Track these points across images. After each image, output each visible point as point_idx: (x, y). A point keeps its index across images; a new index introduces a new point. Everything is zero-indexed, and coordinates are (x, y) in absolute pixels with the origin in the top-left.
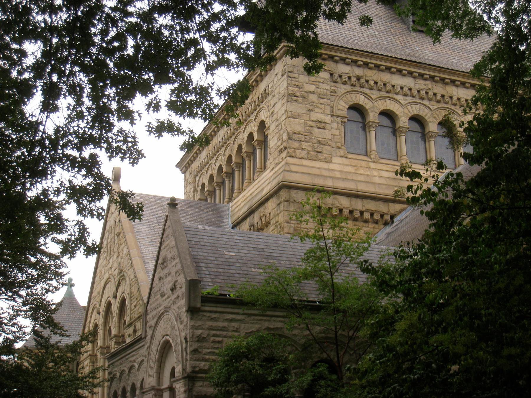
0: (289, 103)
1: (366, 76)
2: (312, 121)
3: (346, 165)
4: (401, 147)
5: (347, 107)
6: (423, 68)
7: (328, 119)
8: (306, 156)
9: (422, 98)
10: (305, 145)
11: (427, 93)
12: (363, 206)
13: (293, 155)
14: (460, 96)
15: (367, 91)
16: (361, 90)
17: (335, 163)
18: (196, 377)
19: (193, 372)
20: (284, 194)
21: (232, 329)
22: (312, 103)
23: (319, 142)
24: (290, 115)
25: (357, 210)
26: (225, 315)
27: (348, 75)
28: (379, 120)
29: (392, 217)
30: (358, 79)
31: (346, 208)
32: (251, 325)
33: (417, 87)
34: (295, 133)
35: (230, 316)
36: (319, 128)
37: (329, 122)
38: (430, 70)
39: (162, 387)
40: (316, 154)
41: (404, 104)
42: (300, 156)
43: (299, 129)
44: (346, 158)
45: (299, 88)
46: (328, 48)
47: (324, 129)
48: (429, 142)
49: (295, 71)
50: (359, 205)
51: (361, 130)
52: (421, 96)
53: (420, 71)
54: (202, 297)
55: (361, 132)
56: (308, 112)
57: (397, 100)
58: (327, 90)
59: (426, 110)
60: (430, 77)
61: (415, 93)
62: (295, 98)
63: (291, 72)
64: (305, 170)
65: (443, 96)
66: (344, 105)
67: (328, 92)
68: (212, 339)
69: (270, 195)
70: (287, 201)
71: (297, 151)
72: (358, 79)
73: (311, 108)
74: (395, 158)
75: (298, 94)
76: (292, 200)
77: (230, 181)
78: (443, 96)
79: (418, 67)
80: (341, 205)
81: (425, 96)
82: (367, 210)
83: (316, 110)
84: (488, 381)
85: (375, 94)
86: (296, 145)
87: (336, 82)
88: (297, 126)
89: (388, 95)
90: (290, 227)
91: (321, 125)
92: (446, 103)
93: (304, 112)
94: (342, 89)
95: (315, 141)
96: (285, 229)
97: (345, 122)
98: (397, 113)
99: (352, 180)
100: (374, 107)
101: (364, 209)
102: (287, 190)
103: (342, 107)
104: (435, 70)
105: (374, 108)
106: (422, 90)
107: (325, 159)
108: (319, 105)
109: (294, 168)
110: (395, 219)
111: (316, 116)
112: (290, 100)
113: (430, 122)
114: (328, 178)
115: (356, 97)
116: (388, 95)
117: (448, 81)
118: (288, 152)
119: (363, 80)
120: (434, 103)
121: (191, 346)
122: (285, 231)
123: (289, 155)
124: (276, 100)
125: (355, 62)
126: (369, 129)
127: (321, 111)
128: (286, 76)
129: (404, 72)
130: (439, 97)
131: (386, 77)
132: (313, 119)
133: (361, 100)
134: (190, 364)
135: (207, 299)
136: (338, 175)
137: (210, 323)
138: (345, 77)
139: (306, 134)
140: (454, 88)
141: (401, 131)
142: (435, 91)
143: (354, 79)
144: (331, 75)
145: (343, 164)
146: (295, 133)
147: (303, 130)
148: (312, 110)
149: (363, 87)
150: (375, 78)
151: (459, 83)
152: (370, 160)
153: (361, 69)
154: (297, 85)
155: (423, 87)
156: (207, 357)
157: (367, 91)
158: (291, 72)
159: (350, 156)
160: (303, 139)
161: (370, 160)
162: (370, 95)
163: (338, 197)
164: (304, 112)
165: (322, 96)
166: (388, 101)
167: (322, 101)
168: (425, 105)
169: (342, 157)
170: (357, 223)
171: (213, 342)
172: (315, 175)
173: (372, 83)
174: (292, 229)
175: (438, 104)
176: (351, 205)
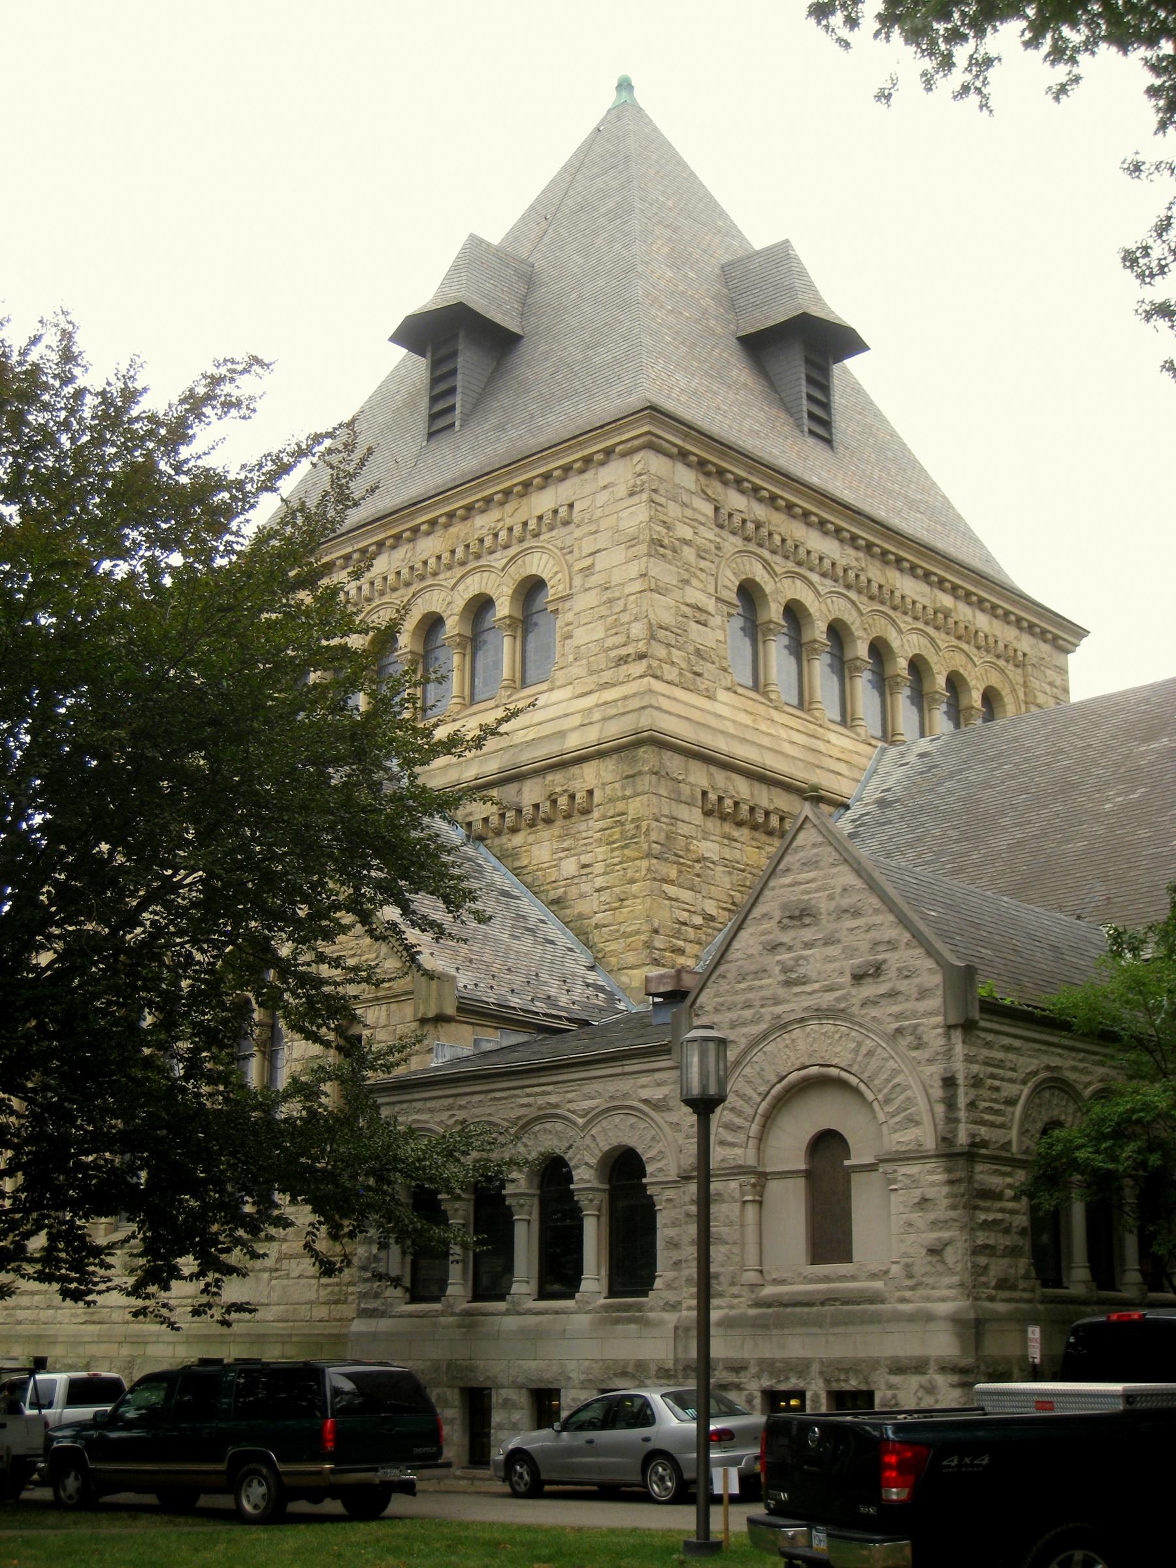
0: (652, 559)
1: (770, 523)
2: (688, 605)
3: (739, 709)
4: (810, 682)
7: (710, 605)
8: (677, 680)
10: (676, 655)
11: (857, 576)
12: (771, 800)
13: (659, 674)
14: (907, 592)
15: (766, 554)
16: (759, 551)
17: (721, 703)
18: (977, 1155)
19: (973, 1145)
20: (648, 757)
21: (1009, 1065)
22: (687, 567)
23: (698, 652)
24: (653, 587)
25: (760, 807)
26: (1001, 1037)
27: (743, 516)
30: (758, 526)
31: (745, 801)
32: (1029, 1060)
33: (844, 562)
34: (661, 627)
35: (1007, 1041)
36: (698, 622)
37: (713, 612)
39: (768, 1170)
40: (691, 680)
42: (669, 678)
43: (668, 618)
44: (735, 692)
45: (668, 528)
46: (722, 453)
47: (705, 625)
48: (851, 678)
49: (662, 491)
50: (764, 797)
54: (980, 1001)
56: (680, 585)
57: (812, 584)
58: (710, 541)
59: (854, 613)
62: (662, 550)
63: (655, 491)
64: (682, 710)
66: (732, 578)
67: (712, 546)
68: (989, 1082)
69: (598, 751)
70: (656, 773)
71: (664, 665)
72: (758, 526)
73: (686, 576)
75: (666, 541)
76: (663, 773)
79: (852, 521)
80: (738, 793)
82: (777, 810)
83: (694, 582)
86: (661, 652)
87: (721, 527)
88: (663, 610)
89: (797, 569)
90: (661, 829)
91: (700, 616)
92: (883, 603)
93: (675, 582)
94: (733, 543)
95: (691, 649)
96: (652, 834)
98: (811, 610)
99: (753, 743)
100: (777, 591)
101: (772, 808)
102: (657, 749)
103: (731, 581)
104: (877, 531)
105: (780, 590)
106: (851, 568)
107: (707, 690)
108: (698, 573)
109: (665, 704)
111: (694, 595)
112: (653, 553)
113: (859, 638)
114: (719, 734)
115: (751, 564)
116: (797, 569)
118: (650, 667)
119: (764, 532)
121: (966, 1094)
122: (653, 838)
123: (650, 672)
124: (602, 541)
125: (756, 489)
126: (764, 635)
127: (700, 586)
128: (645, 496)
130: (875, 589)
131: (797, 531)
132: (689, 601)
133: (759, 573)
134: (967, 1130)
135: (991, 1008)
136: (729, 727)
137: (986, 1052)
138: (737, 519)
139: (679, 631)
140: (897, 574)
141: (815, 650)
142: (870, 575)
143: (750, 526)
144: (717, 509)
145: (733, 706)
146: (661, 627)
147: (673, 623)
148: (687, 582)
154: (665, 522)
155: (854, 563)
156: (987, 1117)
157: (766, 554)
158: (655, 491)
160: (673, 643)
162: (774, 565)
163: (734, 776)
164: (675, 582)
165: (703, 554)
167: (703, 564)
168: (853, 602)
169: (728, 689)
170: (757, 834)
171: (990, 1089)
172: (697, 723)
173: (777, 539)
174: (663, 835)
175: (871, 603)
176: (752, 795)
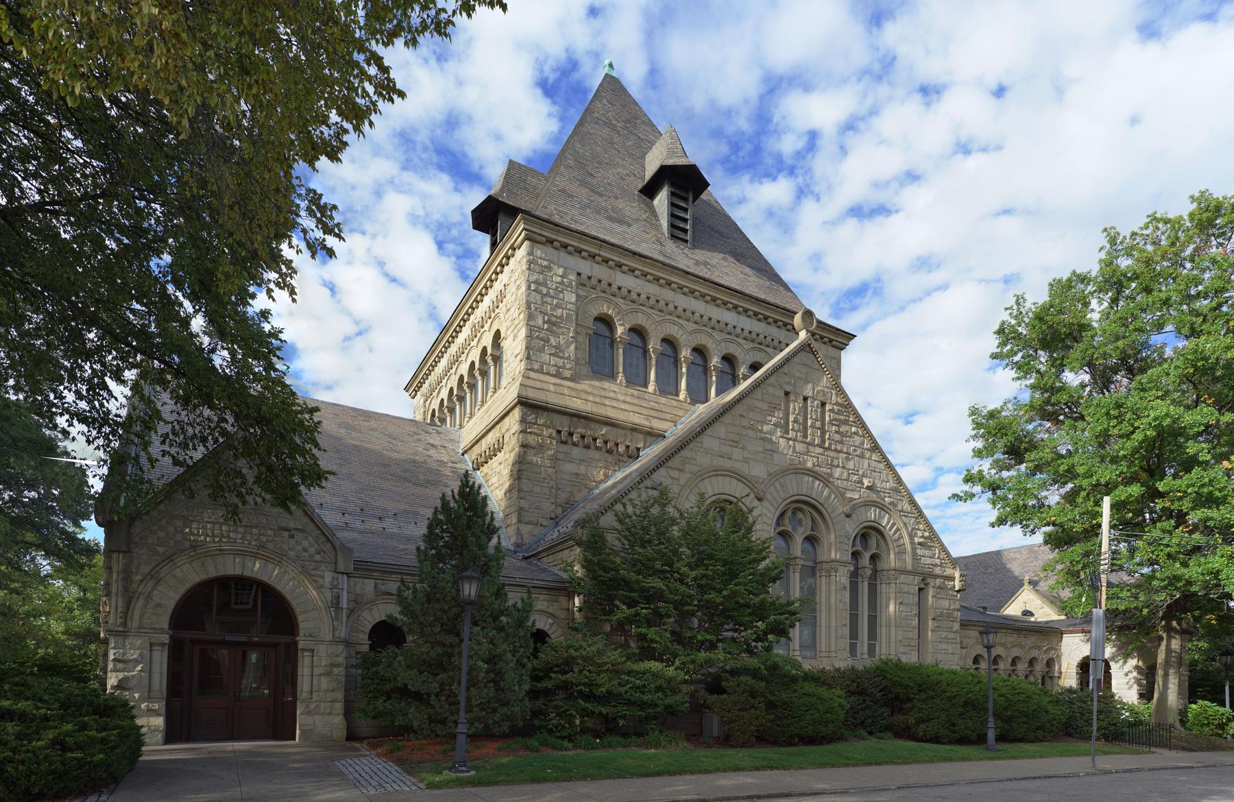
85: (691, 326)
120: (692, 324)
131: (667, 294)
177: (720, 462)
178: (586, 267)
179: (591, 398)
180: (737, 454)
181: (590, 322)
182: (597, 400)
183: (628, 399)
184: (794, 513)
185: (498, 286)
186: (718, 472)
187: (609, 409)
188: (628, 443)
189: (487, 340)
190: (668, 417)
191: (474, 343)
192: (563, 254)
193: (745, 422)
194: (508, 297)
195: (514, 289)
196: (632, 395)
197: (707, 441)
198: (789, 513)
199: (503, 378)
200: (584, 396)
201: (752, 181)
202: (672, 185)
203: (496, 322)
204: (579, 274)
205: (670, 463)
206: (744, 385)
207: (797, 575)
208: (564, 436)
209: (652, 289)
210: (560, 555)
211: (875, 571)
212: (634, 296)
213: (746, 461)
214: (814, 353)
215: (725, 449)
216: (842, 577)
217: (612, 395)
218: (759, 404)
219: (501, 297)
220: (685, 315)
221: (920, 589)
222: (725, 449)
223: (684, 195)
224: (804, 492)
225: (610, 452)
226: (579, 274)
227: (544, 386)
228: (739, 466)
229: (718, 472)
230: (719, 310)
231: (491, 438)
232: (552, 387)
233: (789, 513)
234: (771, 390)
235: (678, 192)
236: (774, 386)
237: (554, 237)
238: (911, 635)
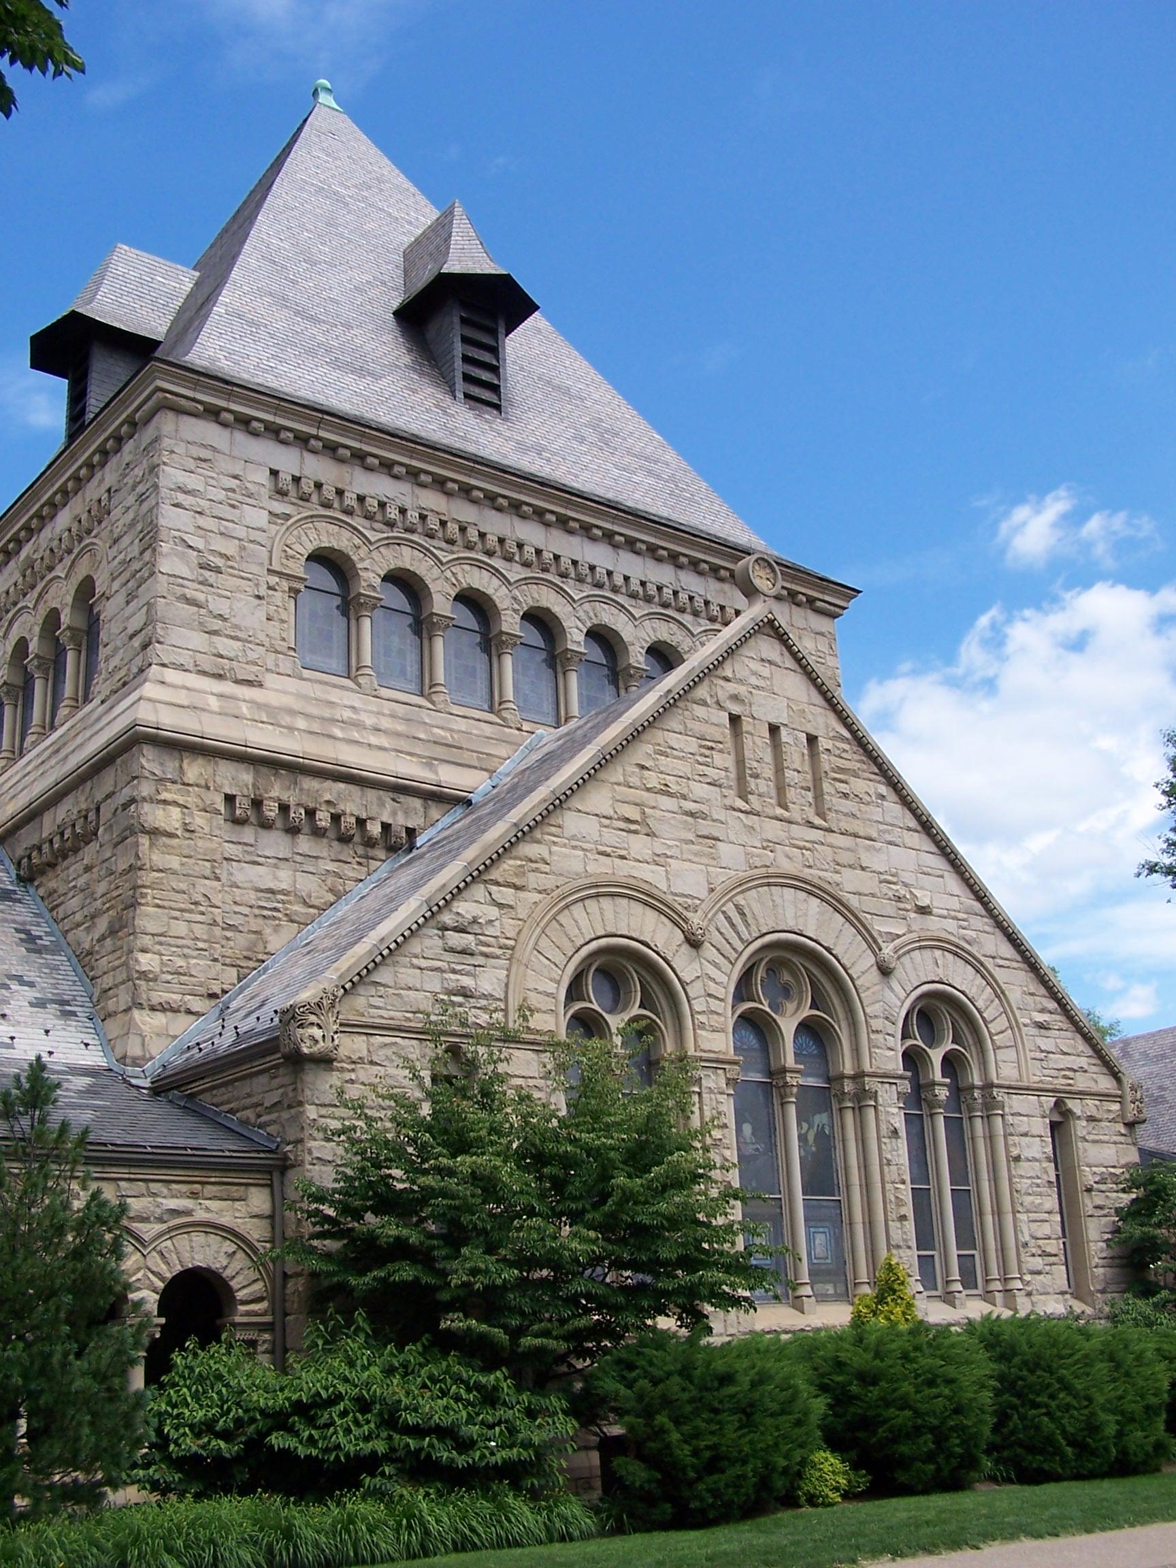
5: (454, 594)
6: (568, 504)
9: (349, 512)
14: (407, 502)
15: (497, 563)
27: (443, 518)
28: (522, 629)
29: (411, 833)
38: (412, 453)
41: (444, 560)
48: (499, 656)
51: (337, 613)
52: (543, 565)
53: (809, 592)
55: (411, 638)
60: (690, 562)
61: (619, 580)
65: (501, 541)
74: (341, 669)
77: (16, 706)
78: (501, 541)
81: (457, 535)
84: (47, 1201)
85: (515, 572)
97: (298, 591)
110: (419, 841)
117: (505, 503)
120: (517, 567)
126: (357, 612)
129: (255, 424)
131: (464, 512)
149: (432, 537)
150: (506, 532)
151: (644, 547)
152: (430, 706)
153: (226, 433)
159: (385, 692)
161: (430, 706)
166: (406, 551)
177: (600, 868)
178: (288, 460)
179: (301, 723)
180: (638, 845)
181: (297, 568)
182: (316, 727)
183: (385, 723)
184: (770, 970)
185: (94, 491)
186: (600, 891)
187: (345, 747)
188: (386, 819)
189: (62, 596)
190: (472, 759)
191: (29, 601)
192: (240, 437)
193: (653, 780)
194: (116, 513)
195: (131, 499)
196: (393, 716)
197: (571, 822)
198: (761, 973)
199: (98, 679)
200: (286, 720)
201: (880, 682)
202: (464, 305)
203: (85, 562)
204: (274, 473)
205: (495, 874)
206: (646, 703)
207: (792, 1110)
208: (242, 805)
209: (431, 500)
210: (245, 1088)
211: (959, 1091)
212: (393, 513)
213: (659, 860)
214: (782, 637)
215: (612, 838)
216: (891, 1109)
217: (347, 714)
218: (674, 740)
219: (101, 513)
220: (505, 550)
221: (1054, 1126)
222: (612, 838)
223: (488, 323)
224: (791, 924)
225: (345, 839)
226: (274, 473)
227: (197, 700)
228: (653, 876)
229: (600, 891)
230: (575, 541)
231: (63, 812)
232: (214, 703)
233: (761, 973)
234: (700, 711)
235: (476, 318)
236: (704, 703)
237: (222, 403)
238: (1046, 1229)
